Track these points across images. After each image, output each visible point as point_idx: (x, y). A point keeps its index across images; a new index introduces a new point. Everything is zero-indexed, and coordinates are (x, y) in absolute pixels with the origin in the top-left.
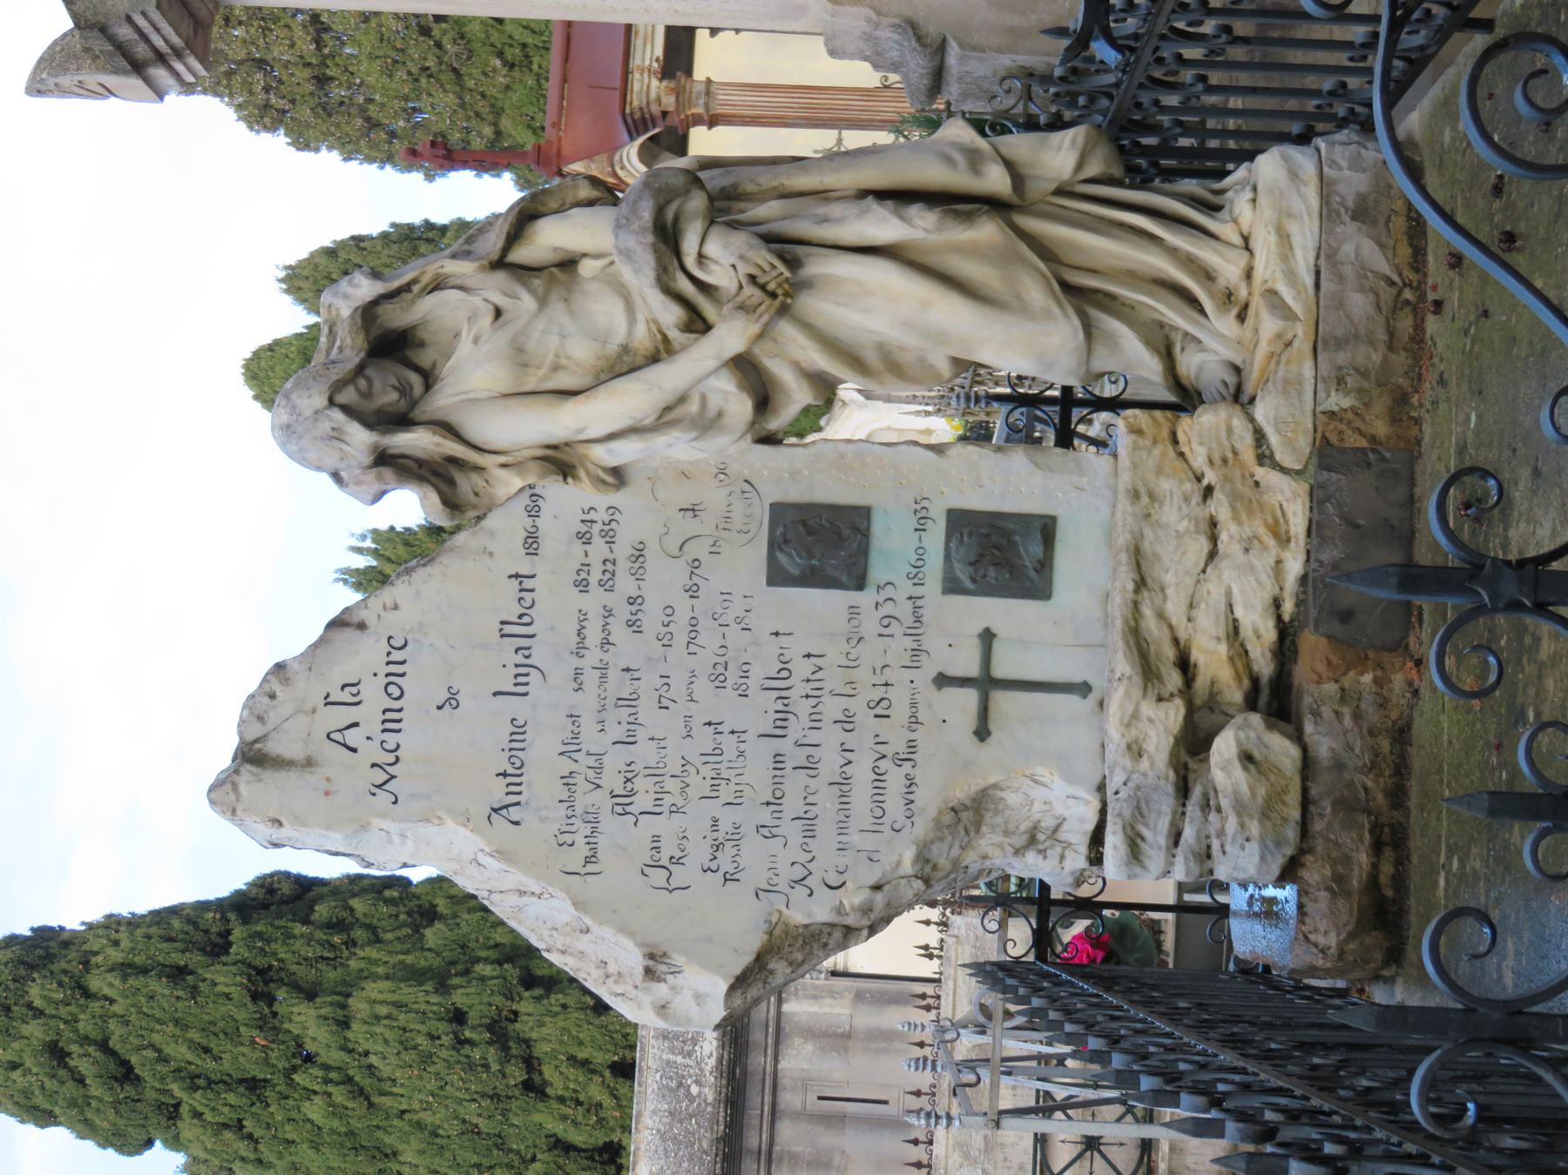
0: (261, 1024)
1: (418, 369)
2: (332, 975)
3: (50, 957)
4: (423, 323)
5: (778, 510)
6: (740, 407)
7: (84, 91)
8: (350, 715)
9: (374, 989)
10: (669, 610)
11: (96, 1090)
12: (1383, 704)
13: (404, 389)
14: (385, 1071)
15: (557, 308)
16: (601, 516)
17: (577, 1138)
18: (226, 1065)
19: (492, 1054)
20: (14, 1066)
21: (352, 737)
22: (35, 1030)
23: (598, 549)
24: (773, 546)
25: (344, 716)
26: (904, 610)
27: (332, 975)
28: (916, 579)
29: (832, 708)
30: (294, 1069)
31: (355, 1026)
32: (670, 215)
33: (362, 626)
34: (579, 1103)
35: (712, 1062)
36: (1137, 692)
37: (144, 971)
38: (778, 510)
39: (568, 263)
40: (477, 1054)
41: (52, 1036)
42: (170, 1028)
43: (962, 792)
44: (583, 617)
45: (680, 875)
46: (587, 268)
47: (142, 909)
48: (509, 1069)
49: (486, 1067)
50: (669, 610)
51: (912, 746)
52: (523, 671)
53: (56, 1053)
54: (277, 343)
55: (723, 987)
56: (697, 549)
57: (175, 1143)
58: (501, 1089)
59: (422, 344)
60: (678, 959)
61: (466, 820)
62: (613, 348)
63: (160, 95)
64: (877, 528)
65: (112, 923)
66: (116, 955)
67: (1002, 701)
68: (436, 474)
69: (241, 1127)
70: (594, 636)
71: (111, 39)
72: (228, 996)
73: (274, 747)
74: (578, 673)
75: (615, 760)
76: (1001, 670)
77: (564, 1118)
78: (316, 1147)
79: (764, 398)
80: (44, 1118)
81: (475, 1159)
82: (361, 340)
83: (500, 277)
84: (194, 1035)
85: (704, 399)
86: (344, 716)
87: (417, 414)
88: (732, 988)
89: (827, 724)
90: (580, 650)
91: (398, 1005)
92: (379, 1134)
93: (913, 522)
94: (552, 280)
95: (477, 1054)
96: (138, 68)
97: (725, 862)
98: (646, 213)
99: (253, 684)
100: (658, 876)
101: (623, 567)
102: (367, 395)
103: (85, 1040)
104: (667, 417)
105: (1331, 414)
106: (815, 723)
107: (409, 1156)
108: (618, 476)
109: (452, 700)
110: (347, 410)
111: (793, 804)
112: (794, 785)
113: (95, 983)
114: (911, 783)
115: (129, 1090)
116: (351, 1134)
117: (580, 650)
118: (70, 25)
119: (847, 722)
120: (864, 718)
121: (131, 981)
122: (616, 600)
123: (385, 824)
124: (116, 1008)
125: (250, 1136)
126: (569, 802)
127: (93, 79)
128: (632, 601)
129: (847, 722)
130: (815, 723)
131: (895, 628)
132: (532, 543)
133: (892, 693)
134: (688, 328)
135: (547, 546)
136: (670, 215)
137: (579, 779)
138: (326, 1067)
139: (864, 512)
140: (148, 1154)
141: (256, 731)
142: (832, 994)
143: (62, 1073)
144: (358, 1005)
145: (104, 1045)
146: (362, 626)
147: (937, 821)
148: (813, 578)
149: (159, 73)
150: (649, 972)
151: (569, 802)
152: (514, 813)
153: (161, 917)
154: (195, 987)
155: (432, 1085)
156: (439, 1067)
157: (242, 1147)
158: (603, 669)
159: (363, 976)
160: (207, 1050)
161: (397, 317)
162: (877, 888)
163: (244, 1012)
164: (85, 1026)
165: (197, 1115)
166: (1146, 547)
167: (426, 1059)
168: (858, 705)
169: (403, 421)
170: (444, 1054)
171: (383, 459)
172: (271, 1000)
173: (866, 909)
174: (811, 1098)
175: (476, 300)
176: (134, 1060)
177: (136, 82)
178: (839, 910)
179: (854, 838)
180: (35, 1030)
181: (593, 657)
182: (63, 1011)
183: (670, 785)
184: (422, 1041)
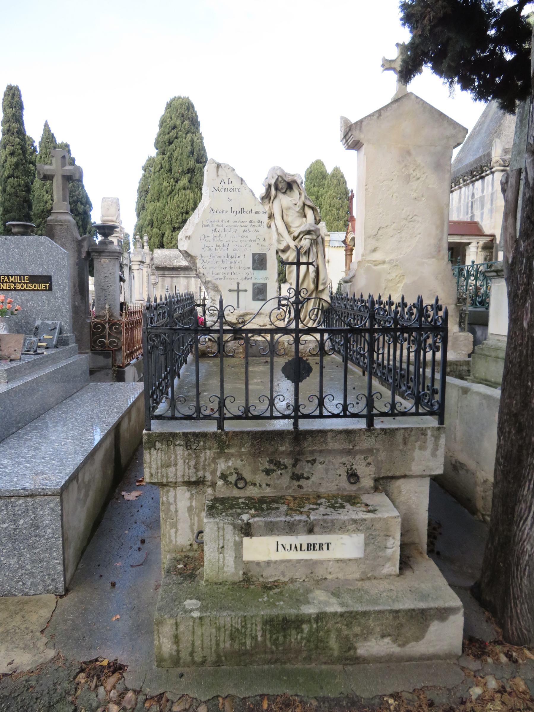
0: (183, 171)
1: (286, 191)
2: (194, 186)
3: (194, 125)
4: (294, 192)
5: (265, 254)
6: (282, 247)
7: (341, 127)
8: (227, 182)
9: (192, 195)
10: (247, 237)
11: (167, 136)
12: (237, 353)
13: (282, 188)
14: (175, 198)
15: (297, 214)
16: (263, 224)
17: (165, 239)
18: (174, 164)
19: (180, 220)
20: (171, 118)
21: (223, 183)
22: (178, 122)
23: (257, 224)
24: (259, 254)
25: (226, 182)
26: (249, 277)
27: (194, 186)
28: (255, 278)
29: (233, 265)
30: (174, 179)
31: (184, 191)
32: (312, 233)
33: (242, 184)
34: (172, 239)
35: (181, 264)
36: (237, 315)
37: (192, 145)
38: (265, 254)
39: (305, 216)
40: (180, 217)
41: (177, 126)
42: (180, 152)
43: (220, 288)
44: (245, 222)
45: (203, 241)
46: (304, 219)
47: (205, 145)
48: (177, 224)
49: (178, 219)
50: (247, 237)
51: (227, 279)
52: (236, 212)
53: (174, 127)
54: (324, 166)
55: (185, 249)
56: (258, 241)
57: (158, 154)
58: (173, 222)
59: (290, 191)
60: (189, 241)
61: (210, 204)
62: (291, 224)
63: (341, 141)
64: (263, 271)
65: (201, 138)
66: (195, 139)
67: (236, 293)
68: (268, 195)
69: (162, 168)
70: (242, 224)
71: (348, 132)
72: (188, 164)
73: (220, 169)
74: (236, 222)
75: (221, 229)
76: (240, 293)
77: (168, 236)
78: (159, 184)
79: (284, 251)
80: (161, 126)
81: (159, 218)
82: (290, 181)
83: (302, 204)
84: (179, 157)
85: (283, 241)
86: (226, 182)
87: (278, 192)
88: (185, 251)
89: (230, 265)
90: (240, 222)
91: (189, 200)
92: (162, 198)
93: (264, 277)
94: (301, 214)
95: (180, 217)
96: (345, 137)
97: (206, 248)
98: (312, 229)
99: (231, 165)
100: (203, 237)
101: (254, 228)
102: (280, 182)
103: (177, 134)
104: (279, 234)
105: (284, 343)
106: (230, 263)
107: (158, 204)
108: (269, 227)
109: (230, 200)
110: (277, 179)
111: (216, 259)
112: (219, 260)
113: (189, 135)
114: (221, 279)
115: (167, 144)
116: (162, 192)
117: (240, 222)
118: (353, 122)
119: (230, 268)
120: (231, 271)
121: (189, 143)
122: (248, 228)
123: (208, 191)
124: (184, 140)
125: (160, 170)
126: (214, 221)
127: (343, 129)
128: (248, 230)
129: (230, 268)
130: (230, 263)
131: (246, 275)
132: (257, 213)
133: (236, 275)
134: (294, 237)
135: (257, 215)
136: (312, 233)
137: (218, 223)
138: (175, 186)
139: (266, 269)
140: (155, 149)
141: (223, 166)
142: (196, 287)
143: (170, 129)
144: (188, 192)
145: (176, 138)
146: (242, 184)
147: (215, 284)
148: (254, 261)
149: (344, 141)
150: (187, 237)
151: (214, 221)
152: (212, 212)
153: (203, 148)
154: (189, 156)
155: (173, 208)
156: (177, 209)
157: (158, 169)
158: (237, 226)
159: (194, 192)
160: (177, 160)
161: (295, 187)
162: (203, 274)
163: (185, 168)
164: (180, 133)
165: (163, 159)
166: (262, 316)
167: (178, 206)
168: (233, 270)
169: (277, 189)
170: (180, 210)
171: (270, 186)
172: (188, 173)
173: (200, 273)
174: (176, 284)
175: (298, 200)
176: (173, 145)
177: (343, 137)
178: (199, 268)
179: (211, 270)
180: (178, 122)
181: (239, 224)
182: (183, 129)
183: (218, 238)
184: (182, 205)
